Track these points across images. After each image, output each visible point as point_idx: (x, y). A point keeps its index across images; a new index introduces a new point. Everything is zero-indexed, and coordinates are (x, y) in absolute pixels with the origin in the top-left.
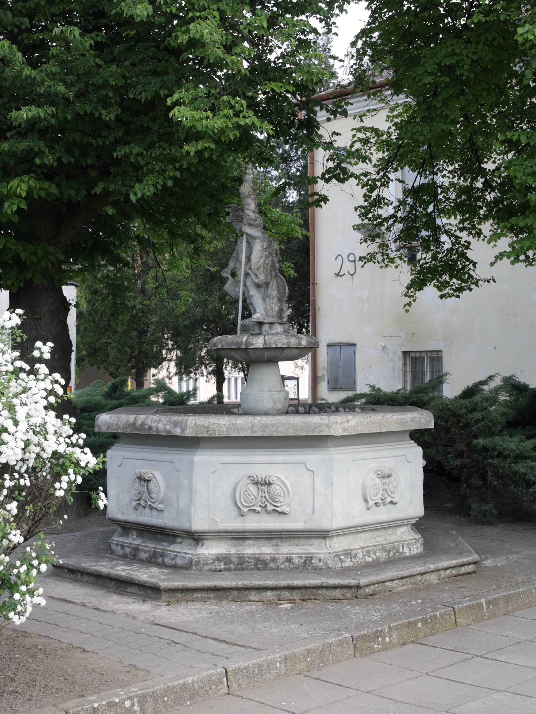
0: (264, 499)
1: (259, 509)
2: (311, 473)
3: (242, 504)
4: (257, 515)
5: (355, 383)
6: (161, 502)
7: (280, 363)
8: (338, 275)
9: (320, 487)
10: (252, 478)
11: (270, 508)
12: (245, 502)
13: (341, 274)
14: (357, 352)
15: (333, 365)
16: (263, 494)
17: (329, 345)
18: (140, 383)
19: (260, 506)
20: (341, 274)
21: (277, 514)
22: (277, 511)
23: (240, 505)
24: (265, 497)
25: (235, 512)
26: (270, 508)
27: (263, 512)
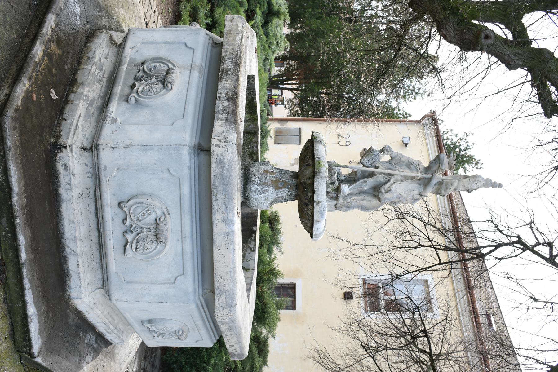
0: (139, 230)
1: (128, 223)
2: (173, 280)
3: (132, 206)
4: (122, 224)
5: (279, 144)
6: (136, 101)
7: (296, 202)
8: (339, 135)
9: (157, 290)
10: (162, 219)
11: (130, 237)
12: (134, 210)
13: (339, 137)
14: (295, 145)
15: (289, 131)
16: (145, 230)
17: (300, 129)
18: (270, 258)
19: (131, 226)
20: (339, 137)
21: (124, 243)
22: (125, 245)
23: (131, 202)
24: (142, 232)
25: (124, 198)
26: (130, 237)
27: (124, 228)
